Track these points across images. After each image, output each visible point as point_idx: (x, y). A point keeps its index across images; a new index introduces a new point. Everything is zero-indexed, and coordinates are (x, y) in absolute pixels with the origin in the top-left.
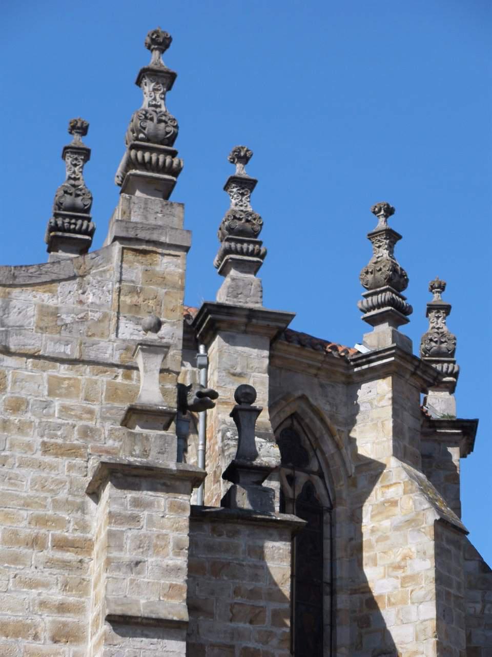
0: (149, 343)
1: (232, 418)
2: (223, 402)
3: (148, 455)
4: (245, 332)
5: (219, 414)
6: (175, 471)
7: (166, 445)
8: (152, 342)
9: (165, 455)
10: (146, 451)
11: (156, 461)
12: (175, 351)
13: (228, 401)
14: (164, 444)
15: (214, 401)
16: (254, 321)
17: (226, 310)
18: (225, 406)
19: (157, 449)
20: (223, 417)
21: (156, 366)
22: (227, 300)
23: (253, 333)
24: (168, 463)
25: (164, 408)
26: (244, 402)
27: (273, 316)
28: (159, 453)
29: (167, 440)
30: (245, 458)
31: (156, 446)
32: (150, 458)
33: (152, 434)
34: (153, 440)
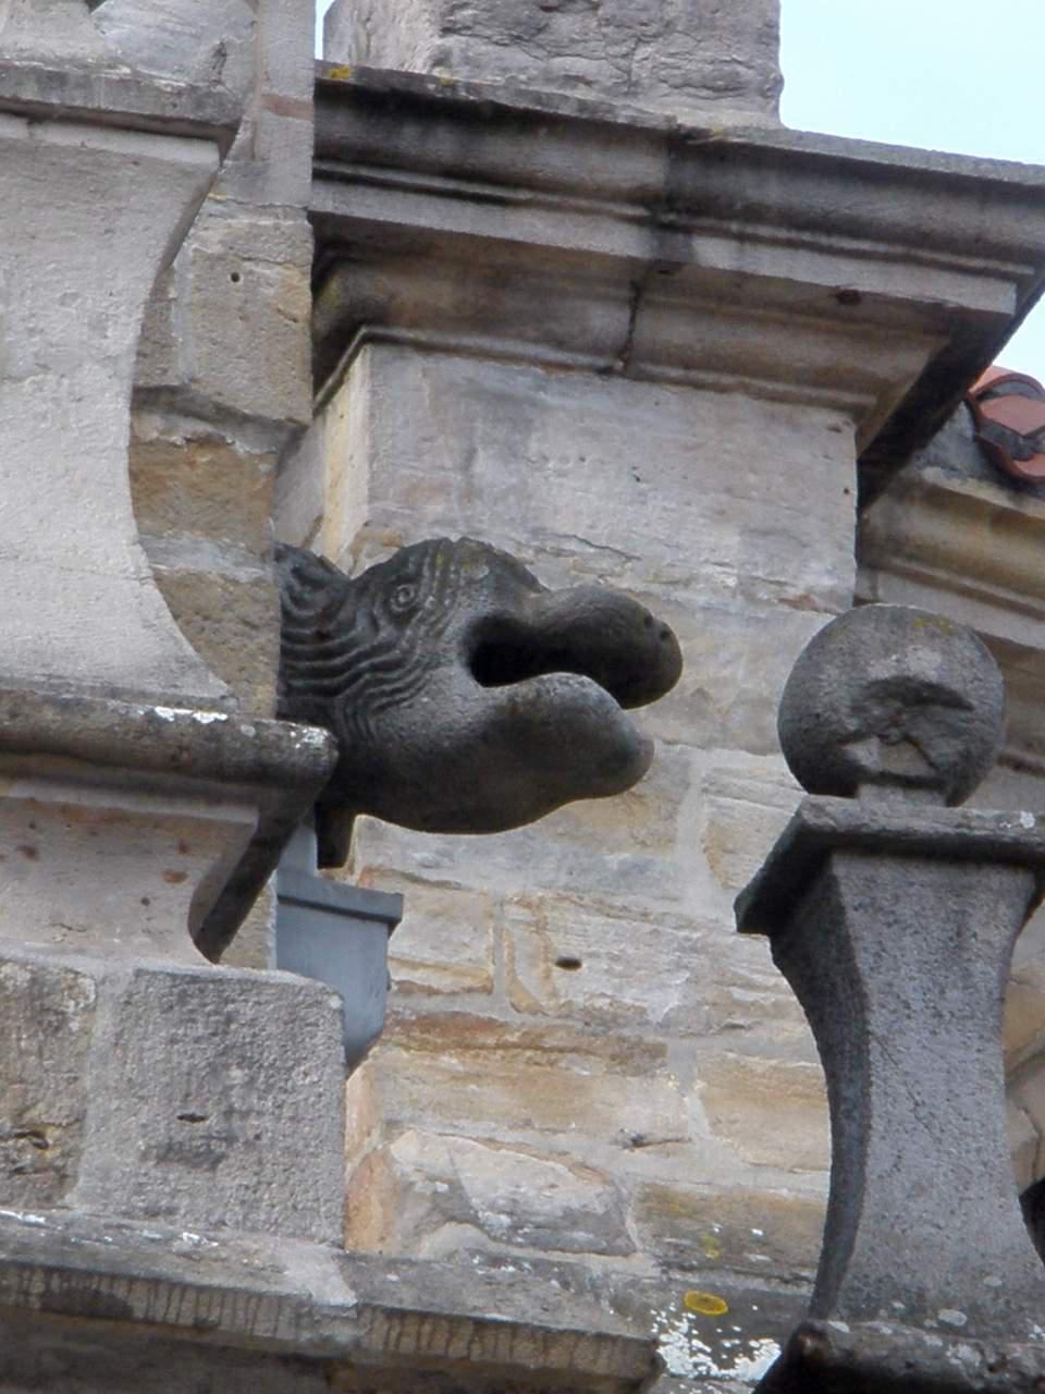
0: (30, 93)
1: (761, 946)
2: (428, 1022)
3: (63, 1178)
4: (625, 362)
5: (392, 1127)
6: (337, 1314)
7: (237, 1075)
8: (57, 79)
9: (231, 1179)
10: (36, 1135)
11: (149, 1230)
12: (243, 221)
13: (476, 1007)
14: (215, 1070)
15: (644, 721)
16: (714, 254)
17: (444, 144)
18: (449, 1061)
19: (151, 1119)
20: (438, 1160)
21: (98, 325)
22: (441, 60)
23: (699, 372)
24: (264, 1247)
25: (206, 718)
26: (884, 779)
27: (892, 208)
28: (168, 1153)
29: (239, 1033)
30: (916, 1311)
31: (132, 1088)
32: (76, 1205)
33: (90, 966)
34: (104, 1024)
